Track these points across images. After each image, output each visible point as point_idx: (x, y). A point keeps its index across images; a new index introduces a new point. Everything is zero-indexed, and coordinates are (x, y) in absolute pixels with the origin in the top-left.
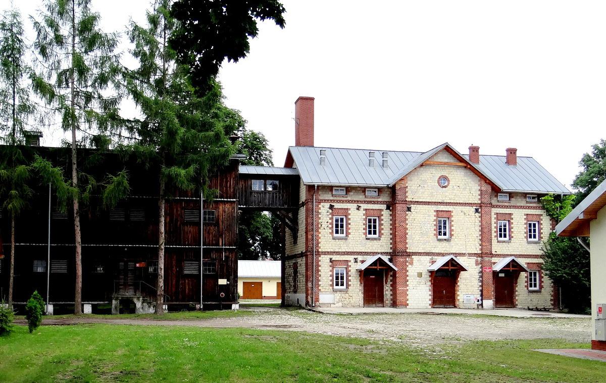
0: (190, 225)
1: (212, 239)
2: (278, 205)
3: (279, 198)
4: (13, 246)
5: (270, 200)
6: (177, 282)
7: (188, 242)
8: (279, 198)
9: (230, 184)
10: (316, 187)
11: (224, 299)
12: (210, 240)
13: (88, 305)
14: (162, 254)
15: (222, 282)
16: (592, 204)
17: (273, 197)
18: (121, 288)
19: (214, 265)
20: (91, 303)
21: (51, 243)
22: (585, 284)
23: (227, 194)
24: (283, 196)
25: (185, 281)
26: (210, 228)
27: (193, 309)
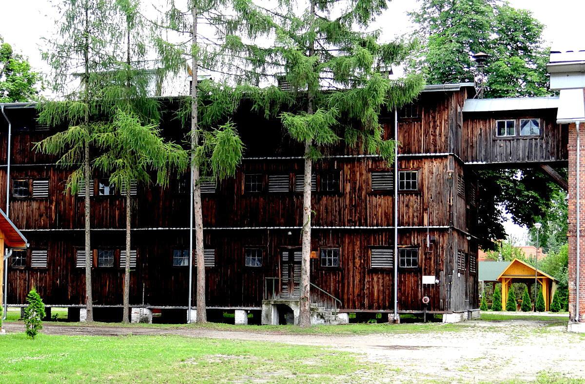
0: (380, 195)
1: (413, 215)
2: (539, 158)
3: (541, 146)
4: (128, 232)
5: (525, 150)
6: (362, 280)
7: (377, 221)
8: (541, 146)
9: (441, 129)
10: (578, 126)
11: (429, 307)
12: (409, 217)
13: (240, 311)
14: (307, 239)
15: (429, 280)
16: (579, 76)
17: (531, 145)
18: (284, 289)
19: (415, 254)
20: (244, 308)
21: (394, 229)
22: (46, 304)
23: (435, 146)
24: (547, 143)
25: (373, 279)
26: (409, 199)
27: (384, 319)
